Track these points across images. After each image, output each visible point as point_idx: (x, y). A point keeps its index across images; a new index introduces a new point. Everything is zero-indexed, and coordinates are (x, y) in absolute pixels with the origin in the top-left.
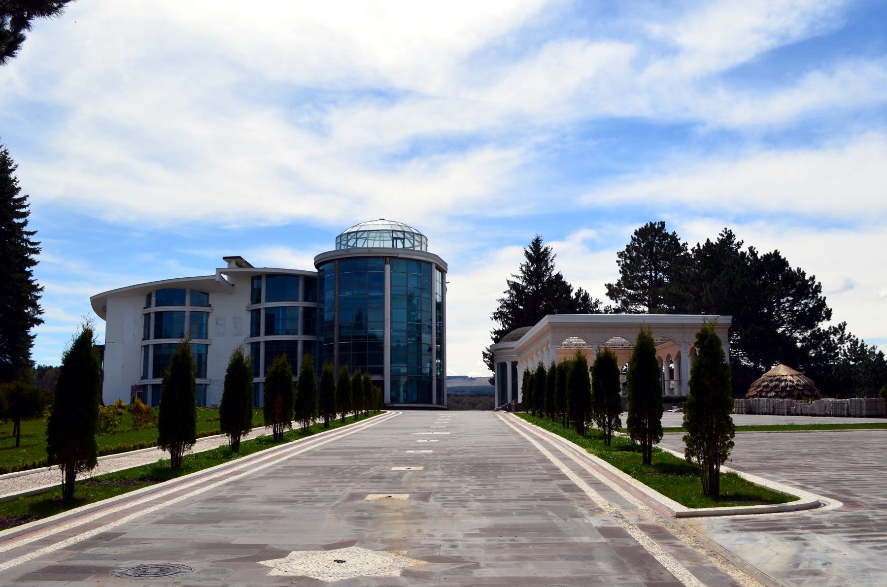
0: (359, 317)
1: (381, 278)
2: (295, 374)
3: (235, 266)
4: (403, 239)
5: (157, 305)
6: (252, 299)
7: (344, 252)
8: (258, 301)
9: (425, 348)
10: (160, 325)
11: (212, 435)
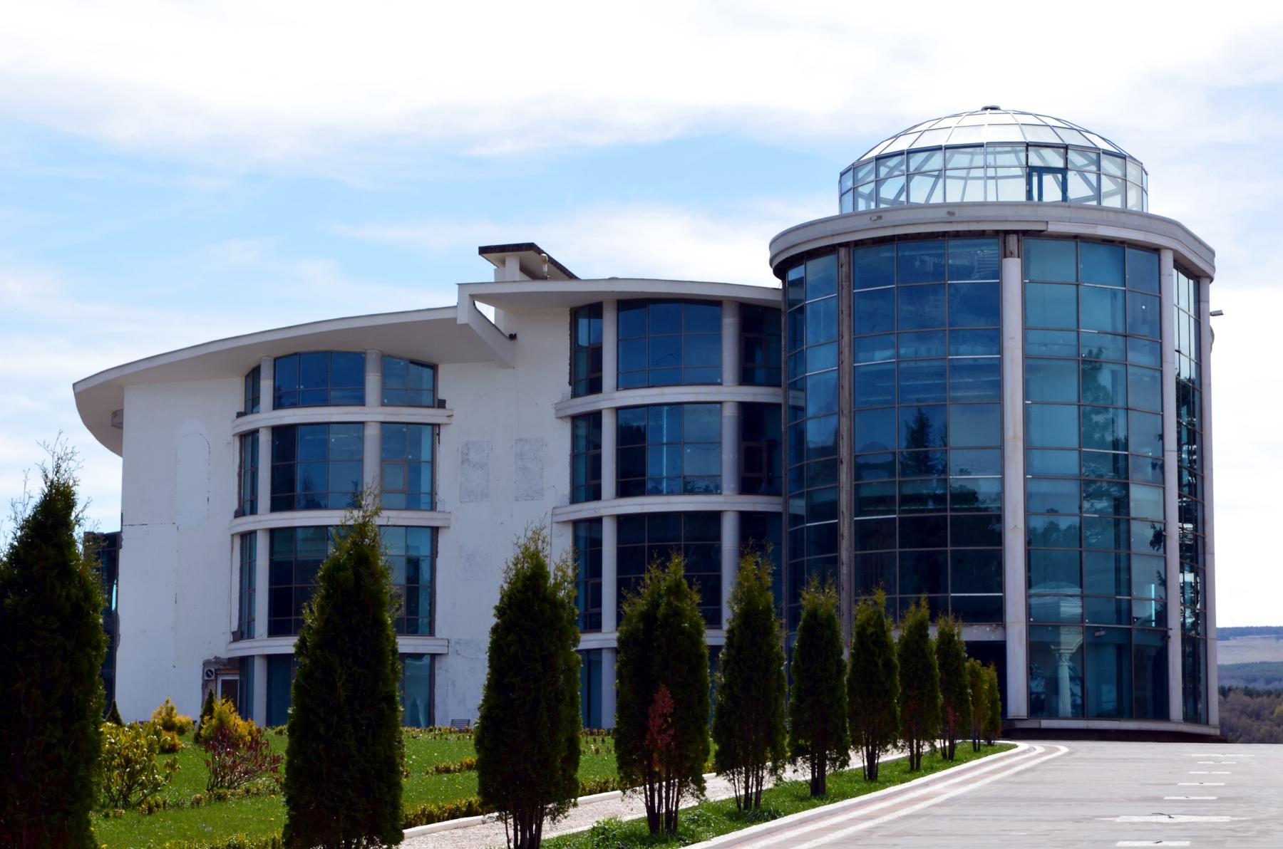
0: (920, 433)
2: (715, 621)
3: (518, 275)
4: (1064, 171)
5: (278, 404)
6: (573, 381)
7: (865, 222)
9: (1141, 534)
10: (288, 468)
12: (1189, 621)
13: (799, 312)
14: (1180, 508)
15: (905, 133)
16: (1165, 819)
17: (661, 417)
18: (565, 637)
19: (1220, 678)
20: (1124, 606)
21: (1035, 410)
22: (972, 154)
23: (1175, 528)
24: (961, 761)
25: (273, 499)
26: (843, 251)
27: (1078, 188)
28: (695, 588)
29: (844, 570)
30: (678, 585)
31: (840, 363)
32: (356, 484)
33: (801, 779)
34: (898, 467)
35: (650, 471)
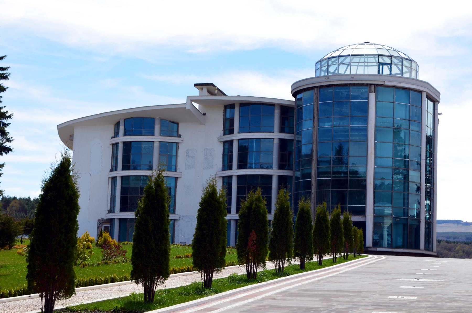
0: (340, 151)
1: (364, 108)
2: (270, 211)
3: (207, 93)
4: (390, 64)
5: (125, 135)
6: (224, 130)
7: (323, 79)
8: (231, 132)
9: (413, 187)
10: (128, 156)
11: (183, 271)
12: (428, 217)
13: (300, 109)
14: (426, 178)
15: (338, 50)
16: (416, 280)
17: (253, 143)
18: (222, 214)
19: (437, 237)
20: (406, 211)
21: (378, 145)
22: (360, 58)
23: (424, 185)
24: (350, 260)
25: (123, 166)
26: (316, 89)
27: (395, 70)
28: (265, 199)
29: (313, 196)
30: (259, 198)
31: (314, 126)
32: (150, 162)
33: (297, 264)
34: (332, 162)
35: (249, 161)
